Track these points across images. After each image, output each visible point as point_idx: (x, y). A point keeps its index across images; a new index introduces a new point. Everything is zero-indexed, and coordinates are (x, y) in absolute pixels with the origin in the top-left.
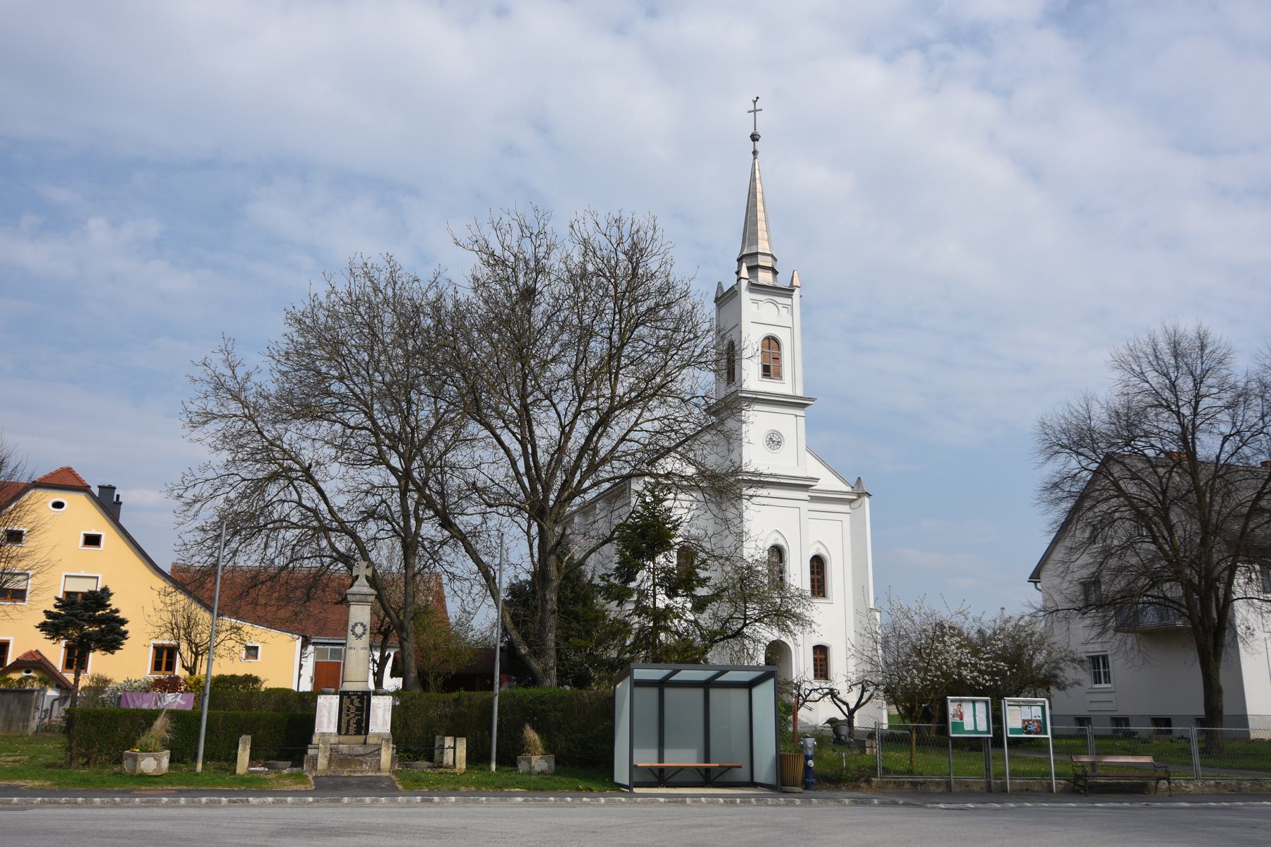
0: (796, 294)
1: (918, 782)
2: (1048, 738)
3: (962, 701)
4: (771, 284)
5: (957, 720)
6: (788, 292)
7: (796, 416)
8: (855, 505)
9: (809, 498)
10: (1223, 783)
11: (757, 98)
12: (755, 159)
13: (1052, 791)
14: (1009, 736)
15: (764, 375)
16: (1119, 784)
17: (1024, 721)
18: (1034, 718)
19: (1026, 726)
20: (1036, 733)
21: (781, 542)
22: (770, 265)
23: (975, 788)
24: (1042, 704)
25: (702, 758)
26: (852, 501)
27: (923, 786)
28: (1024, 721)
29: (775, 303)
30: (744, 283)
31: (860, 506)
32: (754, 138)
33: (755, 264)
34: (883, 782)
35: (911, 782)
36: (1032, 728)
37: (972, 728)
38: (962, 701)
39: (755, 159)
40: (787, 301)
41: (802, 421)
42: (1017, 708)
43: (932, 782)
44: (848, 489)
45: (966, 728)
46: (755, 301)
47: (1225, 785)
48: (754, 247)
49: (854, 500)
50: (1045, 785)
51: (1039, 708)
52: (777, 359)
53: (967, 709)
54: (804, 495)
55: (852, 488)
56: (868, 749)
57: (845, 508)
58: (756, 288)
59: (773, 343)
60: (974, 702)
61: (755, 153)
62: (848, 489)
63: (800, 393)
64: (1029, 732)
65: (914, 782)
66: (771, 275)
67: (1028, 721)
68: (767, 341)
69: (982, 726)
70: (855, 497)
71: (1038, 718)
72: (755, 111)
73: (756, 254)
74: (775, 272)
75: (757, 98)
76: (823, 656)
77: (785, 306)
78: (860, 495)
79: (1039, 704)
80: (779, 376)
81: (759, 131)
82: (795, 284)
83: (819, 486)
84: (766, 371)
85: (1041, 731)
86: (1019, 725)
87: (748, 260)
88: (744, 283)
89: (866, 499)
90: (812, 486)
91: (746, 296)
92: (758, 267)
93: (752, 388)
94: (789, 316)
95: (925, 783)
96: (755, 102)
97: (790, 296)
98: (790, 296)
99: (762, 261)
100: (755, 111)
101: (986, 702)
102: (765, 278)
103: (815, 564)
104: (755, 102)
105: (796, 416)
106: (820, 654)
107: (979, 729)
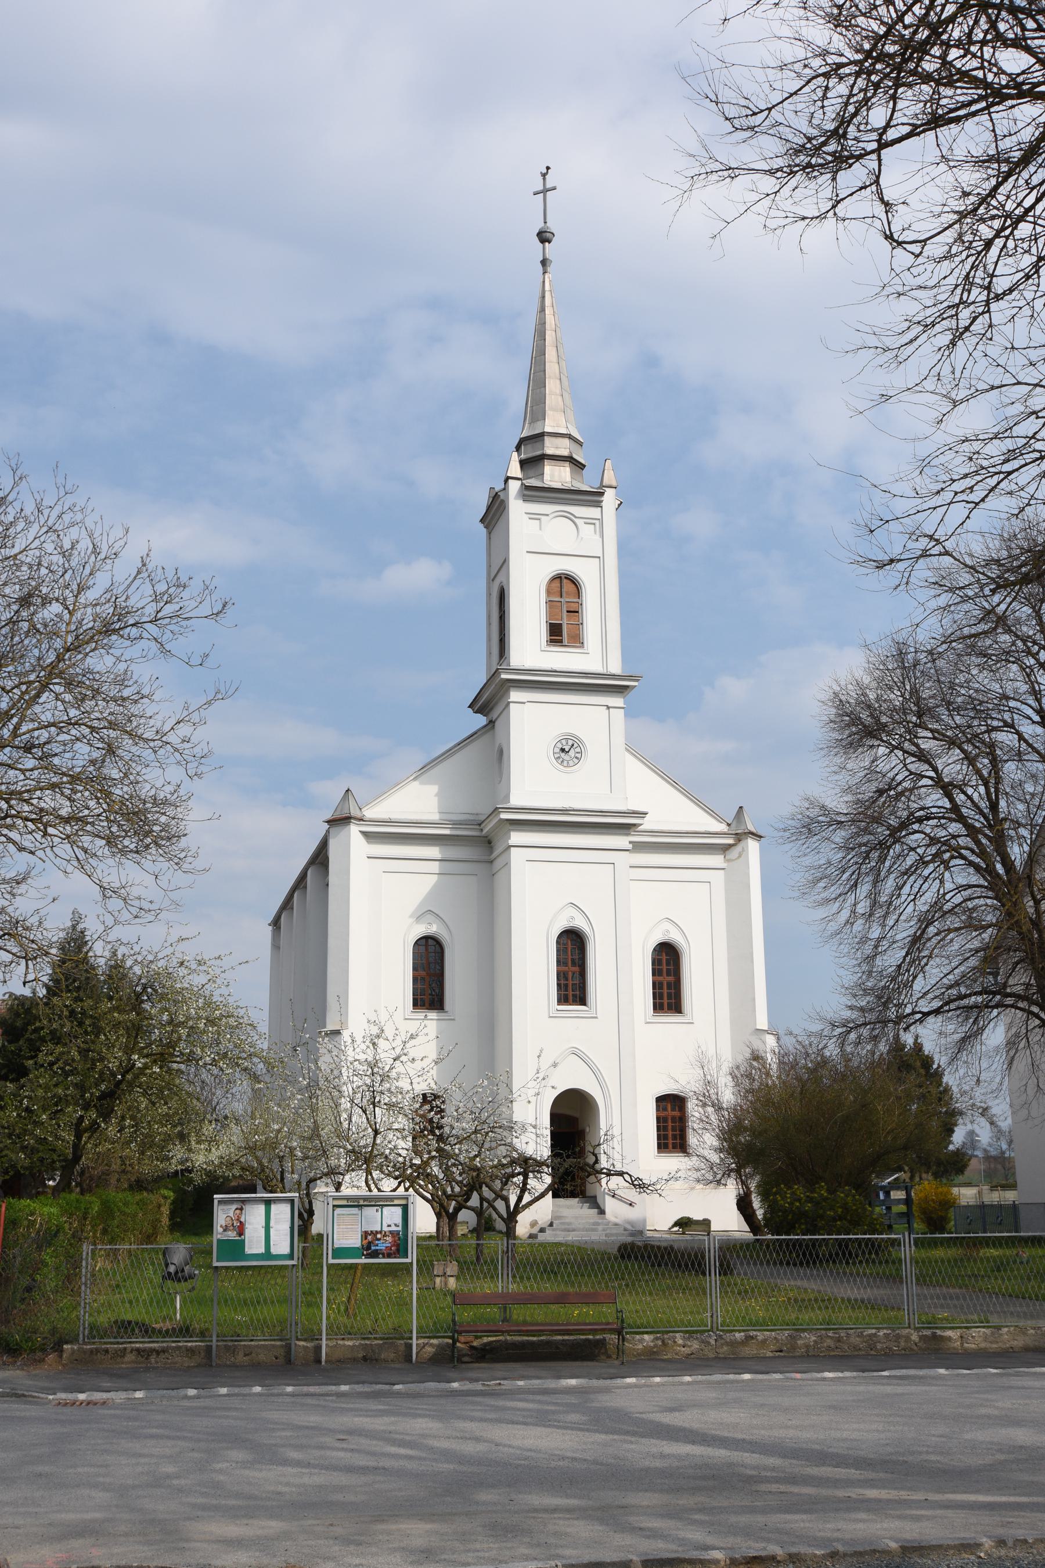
0: (609, 498)
1: (153, 1350)
2: (408, 1267)
3: (244, 1201)
4: (568, 486)
5: (232, 1235)
6: (593, 497)
7: (608, 708)
8: (734, 853)
9: (630, 847)
10: (760, 1336)
11: (548, 168)
12: (545, 273)
13: (411, 1361)
14: (331, 1261)
15: (552, 641)
16: (548, 1343)
17: (366, 1234)
18: (385, 1229)
19: (370, 1243)
20: (389, 1256)
21: (580, 923)
22: (566, 453)
23: (262, 1357)
24: (403, 1202)
25: (690, 1280)
26: (725, 849)
27: (162, 1356)
28: (366, 1234)
29: (571, 518)
30: (514, 486)
31: (740, 856)
32: (544, 237)
33: (539, 453)
34: (85, 1352)
35: (138, 1350)
36: (381, 1246)
37: (261, 1250)
38: (244, 1201)
39: (545, 273)
40: (593, 512)
41: (618, 715)
42: (355, 1210)
43: (179, 1348)
44: (722, 827)
45: (249, 1250)
46: (535, 517)
47: (764, 1341)
48: (539, 423)
49: (730, 846)
50: (402, 1348)
51: (398, 1211)
52: (575, 612)
53: (254, 1216)
54: (622, 841)
55: (729, 825)
56: (438, 1280)
57: (717, 860)
58: (534, 493)
59: (567, 586)
60: (268, 1203)
61: (544, 262)
62: (722, 827)
63: (615, 667)
64: (375, 1254)
65: (144, 1350)
66: (568, 469)
67: (374, 1233)
68: (557, 583)
69: (281, 1244)
70: (731, 841)
71: (393, 1228)
72: (545, 191)
73: (542, 435)
74: (578, 466)
75: (548, 168)
76: (677, 1113)
77: (589, 521)
78: (739, 837)
79: (396, 1202)
80: (577, 640)
81: (552, 226)
82: (606, 482)
83: (647, 824)
84: (555, 634)
85: (398, 1250)
86: (355, 1241)
87: (529, 447)
88: (514, 486)
89: (752, 845)
90: (634, 825)
91: (517, 509)
92: (542, 458)
93: (529, 664)
94: (597, 537)
95: (164, 1351)
96: (544, 175)
97: (598, 504)
98: (598, 504)
99: (551, 447)
100: (545, 191)
101: (292, 1202)
102: (556, 475)
103: (664, 957)
104: (544, 175)
105: (608, 708)
106: (673, 1110)
107: (274, 1251)
